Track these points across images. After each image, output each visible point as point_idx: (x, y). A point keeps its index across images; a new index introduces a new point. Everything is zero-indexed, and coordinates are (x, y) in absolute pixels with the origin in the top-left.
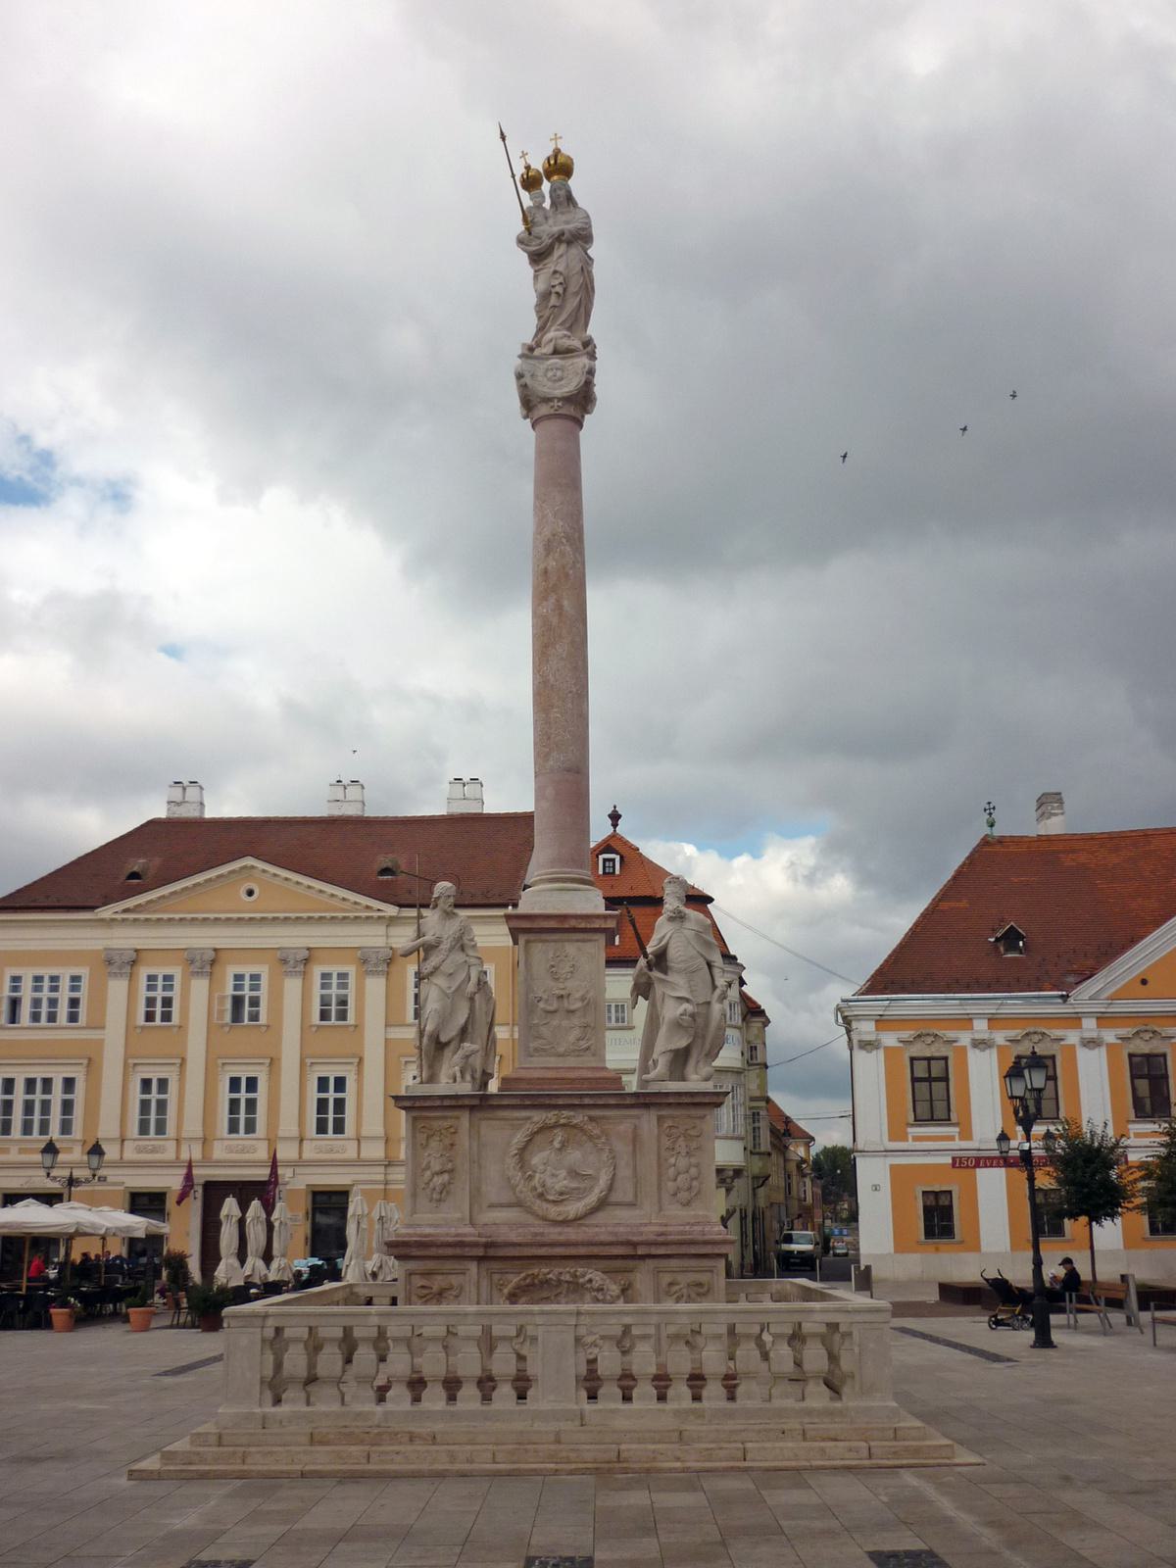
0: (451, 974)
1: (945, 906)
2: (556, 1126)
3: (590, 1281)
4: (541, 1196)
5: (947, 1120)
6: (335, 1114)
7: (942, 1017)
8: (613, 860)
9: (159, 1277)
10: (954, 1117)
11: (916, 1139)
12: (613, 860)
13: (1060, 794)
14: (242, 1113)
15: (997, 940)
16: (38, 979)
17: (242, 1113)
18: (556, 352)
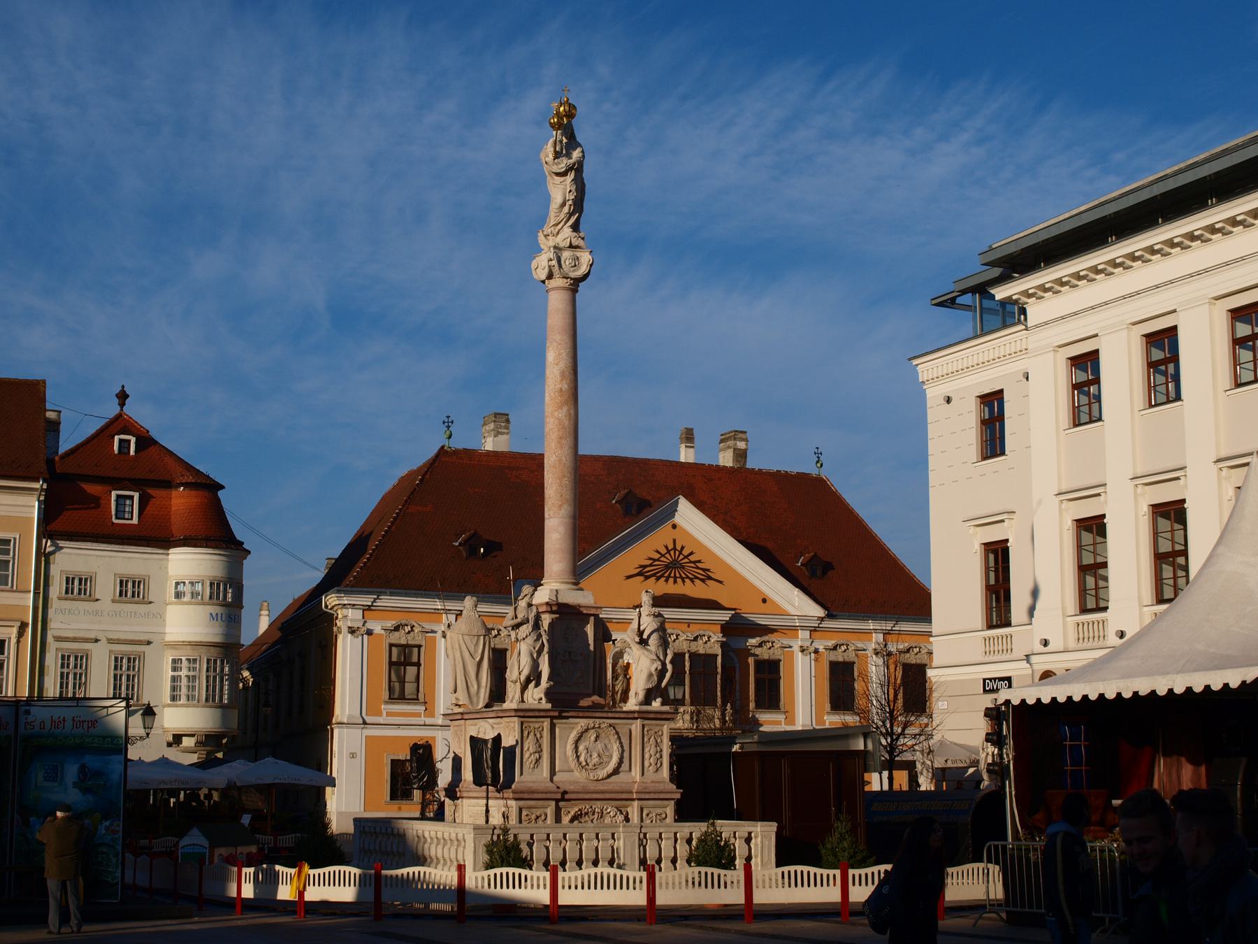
5: (415, 700)
7: (411, 610)
9: (512, 860)
10: (421, 696)
11: (389, 714)
13: (508, 415)
15: (460, 544)
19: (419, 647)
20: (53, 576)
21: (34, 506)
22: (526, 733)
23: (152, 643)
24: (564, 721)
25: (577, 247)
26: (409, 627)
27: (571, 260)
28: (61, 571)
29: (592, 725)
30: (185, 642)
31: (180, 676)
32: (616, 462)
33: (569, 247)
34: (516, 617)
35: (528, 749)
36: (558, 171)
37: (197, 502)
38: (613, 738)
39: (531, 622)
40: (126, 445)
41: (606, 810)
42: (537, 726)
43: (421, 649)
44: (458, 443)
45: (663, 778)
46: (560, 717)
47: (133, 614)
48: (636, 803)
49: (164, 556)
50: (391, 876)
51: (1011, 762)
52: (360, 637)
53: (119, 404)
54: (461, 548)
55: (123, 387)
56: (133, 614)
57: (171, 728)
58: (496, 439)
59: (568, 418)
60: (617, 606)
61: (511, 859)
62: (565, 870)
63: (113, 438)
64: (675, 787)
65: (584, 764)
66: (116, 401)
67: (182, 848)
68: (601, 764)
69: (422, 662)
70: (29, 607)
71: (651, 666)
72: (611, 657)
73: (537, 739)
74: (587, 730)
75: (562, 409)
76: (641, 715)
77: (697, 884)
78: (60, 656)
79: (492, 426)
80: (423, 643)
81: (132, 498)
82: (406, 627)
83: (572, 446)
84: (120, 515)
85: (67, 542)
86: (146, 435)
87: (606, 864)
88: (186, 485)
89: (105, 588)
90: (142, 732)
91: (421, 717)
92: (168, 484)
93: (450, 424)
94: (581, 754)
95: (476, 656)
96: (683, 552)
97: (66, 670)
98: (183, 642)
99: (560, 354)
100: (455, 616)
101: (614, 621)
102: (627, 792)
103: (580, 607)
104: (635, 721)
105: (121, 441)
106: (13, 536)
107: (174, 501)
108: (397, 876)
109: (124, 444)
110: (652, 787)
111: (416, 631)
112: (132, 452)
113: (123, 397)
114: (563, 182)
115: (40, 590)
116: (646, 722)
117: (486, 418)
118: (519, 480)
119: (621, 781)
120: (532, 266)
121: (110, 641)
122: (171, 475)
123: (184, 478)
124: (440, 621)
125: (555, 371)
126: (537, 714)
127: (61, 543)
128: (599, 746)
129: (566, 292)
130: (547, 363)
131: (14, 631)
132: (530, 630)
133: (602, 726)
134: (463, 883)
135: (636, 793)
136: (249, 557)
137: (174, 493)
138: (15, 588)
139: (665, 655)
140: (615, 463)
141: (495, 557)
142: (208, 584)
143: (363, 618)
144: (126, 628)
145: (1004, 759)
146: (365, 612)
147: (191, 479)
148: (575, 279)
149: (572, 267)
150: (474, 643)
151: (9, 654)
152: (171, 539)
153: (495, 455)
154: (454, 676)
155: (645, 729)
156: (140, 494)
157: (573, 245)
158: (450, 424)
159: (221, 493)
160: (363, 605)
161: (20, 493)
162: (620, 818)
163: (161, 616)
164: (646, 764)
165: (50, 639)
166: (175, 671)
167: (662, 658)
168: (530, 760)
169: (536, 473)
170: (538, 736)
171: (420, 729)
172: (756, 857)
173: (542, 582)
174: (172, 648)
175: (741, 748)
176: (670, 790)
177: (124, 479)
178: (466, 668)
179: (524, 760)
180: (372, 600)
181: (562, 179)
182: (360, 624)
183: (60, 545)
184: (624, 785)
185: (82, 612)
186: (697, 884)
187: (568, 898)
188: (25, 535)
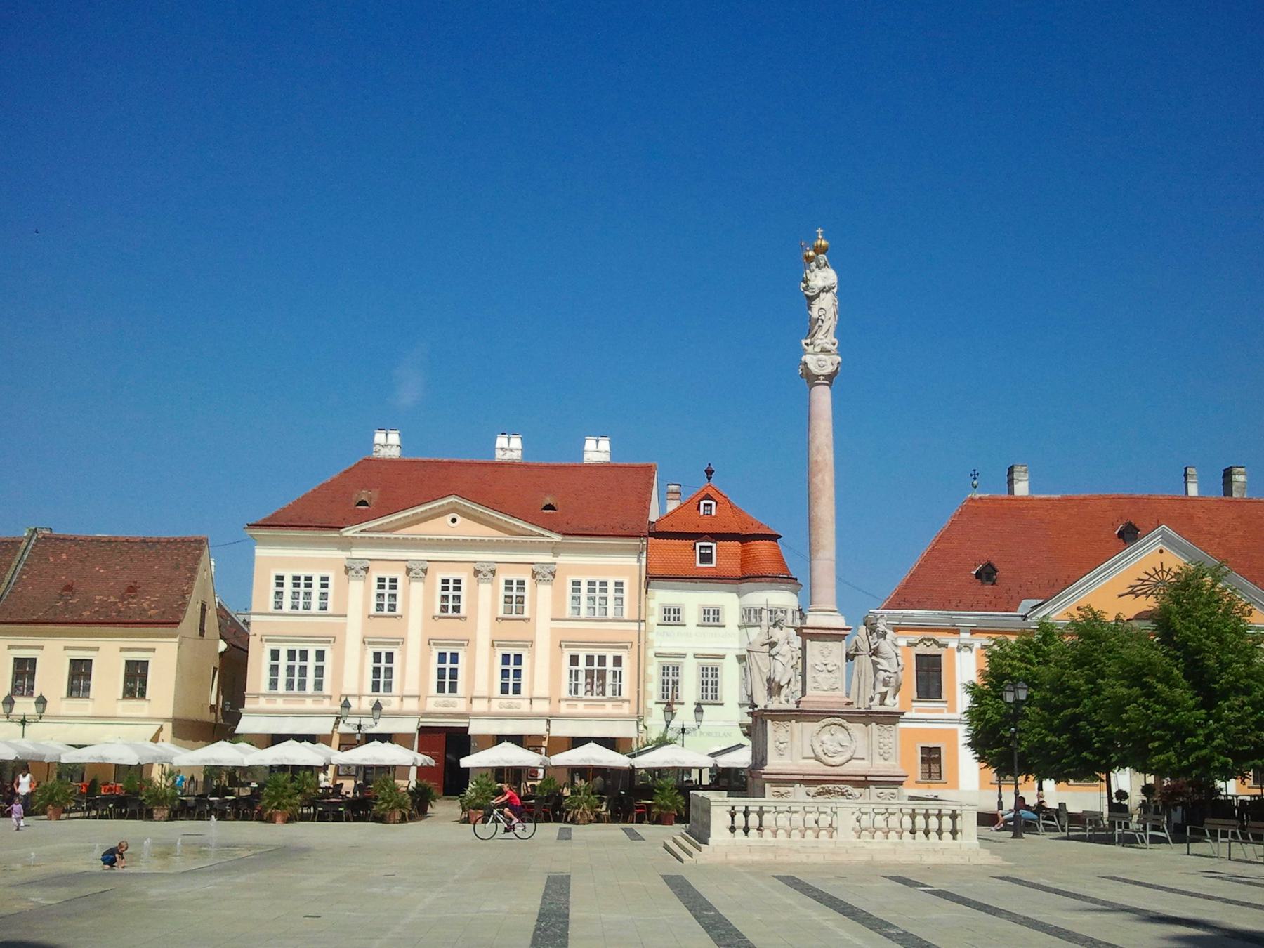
0: (784, 656)
1: (941, 545)
2: (831, 724)
3: (847, 791)
4: (825, 754)
8: (711, 505)
11: (918, 711)
12: (711, 505)
14: (447, 681)
16: (591, 583)
17: (447, 681)
18: (822, 351)
33: (821, 351)
89: (692, 615)
90: (695, 724)
96: (1152, 574)
121: (696, 656)
177: (705, 534)
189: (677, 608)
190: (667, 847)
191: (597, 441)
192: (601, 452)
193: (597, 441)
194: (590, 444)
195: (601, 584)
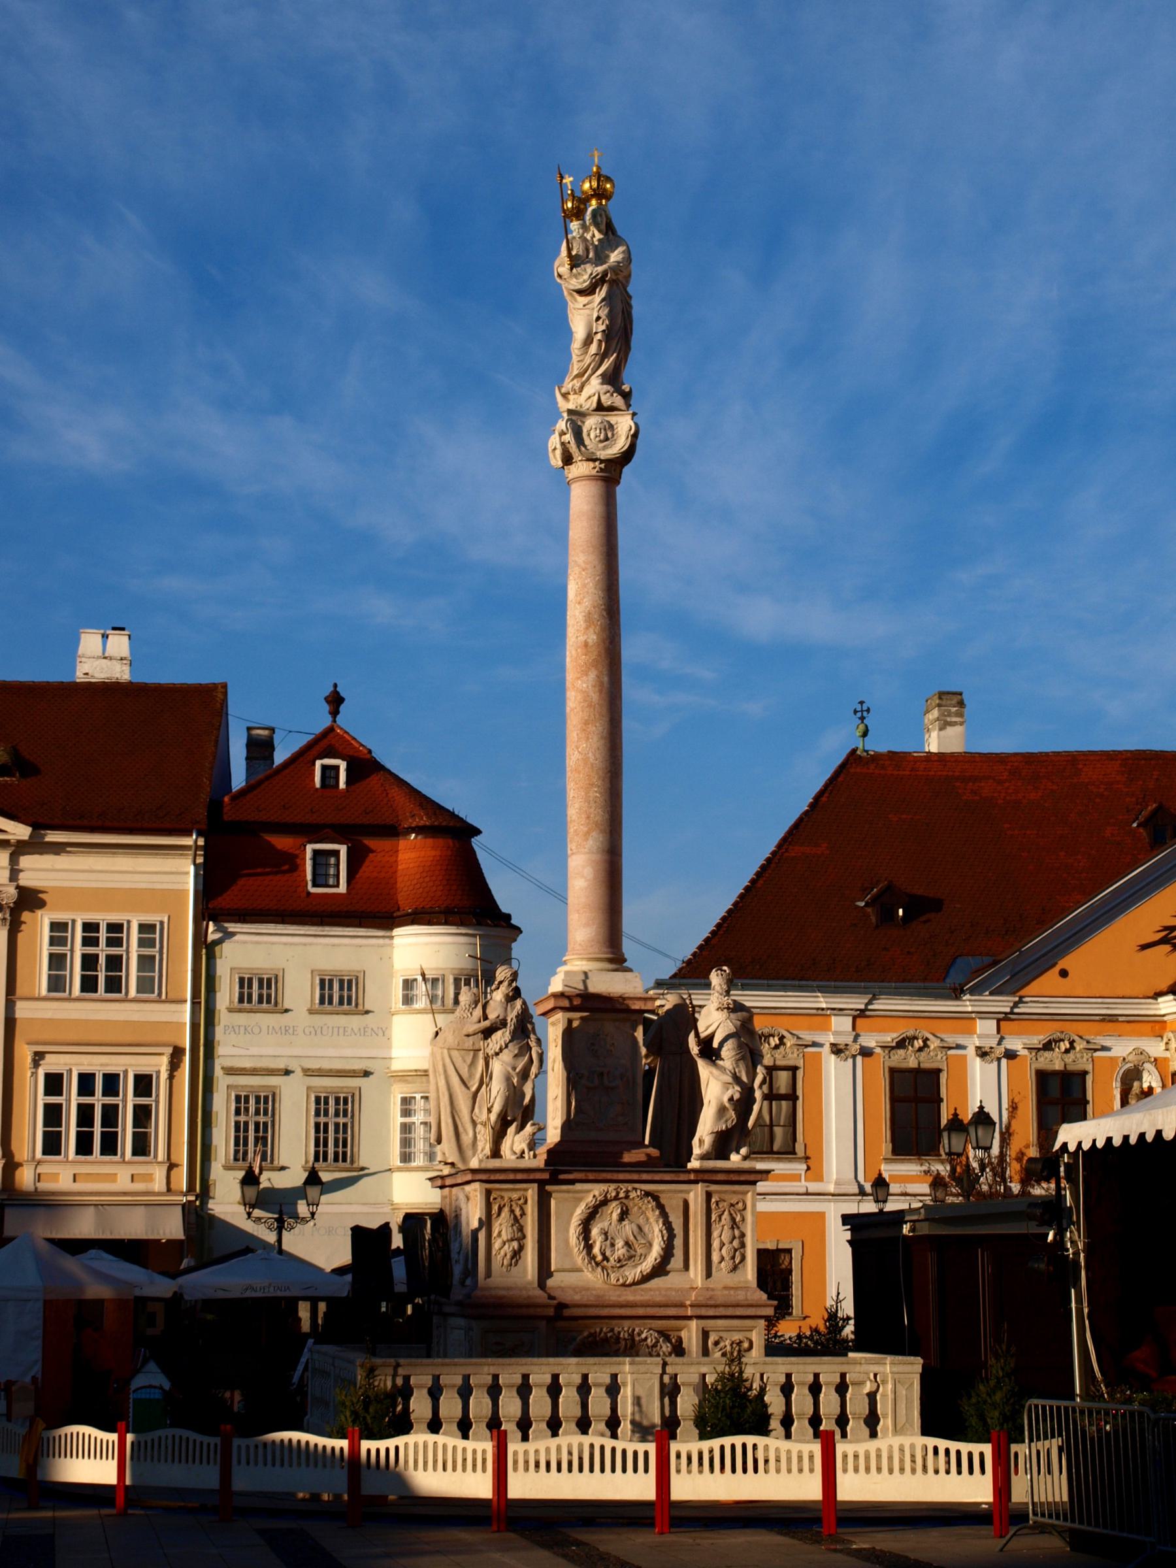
6: (102, 1126)
7: (778, 1011)
10: (799, 1148)
13: (961, 694)
15: (867, 904)
16: (90, 927)
19: (794, 1069)
20: (220, 977)
21: (188, 873)
22: (495, 1208)
23: (372, 1073)
24: (564, 1187)
25: (612, 409)
26: (776, 1039)
27: (598, 431)
28: (231, 969)
29: (614, 1194)
30: (420, 1071)
31: (414, 1123)
32: (1145, 759)
34: (486, 1018)
35: (499, 1234)
36: (579, 287)
37: (434, 856)
38: (653, 1215)
39: (511, 1026)
40: (333, 774)
41: (639, 1335)
42: (515, 1196)
43: (798, 1072)
44: (878, 744)
45: (747, 1281)
46: (555, 1181)
47: (341, 1030)
48: (694, 1324)
49: (387, 941)
50: (274, 1442)
51: (1082, 1255)
52: (996, 1063)
53: (330, 713)
54: (869, 910)
55: (335, 686)
56: (341, 1030)
57: (403, 1204)
58: (942, 733)
59: (597, 689)
60: (1128, 995)
61: (368, 1418)
62: (788, 1436)
63: (314, 764)
64: (765, 1296)
65: (599, 1258)
66: (326, 708)
67: (134, 1391)
68: (631, 1256)
69: (799, 1093)
70: (186, 1023)
71: (723, 1093)
72: (1119, 1080)
73: (515, 1217)
74: (605, 1202)
75: (587, 675)
76: (700, 1176)
77: (565, 1466)
78: (233, 1097)
79: (935, 713)
80: (800, 1063)
81: (336, 853)
82: (771, 1039)
83: (605, 734)
84: (320, 880)
85: (239, 925)
86: (368, 756)
87: (573, 1426)
88: (419, 830)
91: (800, 1181)
92: (393, 831)
93: (865, 714)
94: (594, 1242)
95: (472, 1083)
97: (242, 1118)
98: (416, 1071)
99: (584, 586)
100: (850, 1019)
101: (1121, 1019)
102: (675, 1306)
103: (624, 999)
104: (692, 1186)
105: (325, 768)
106: (159, 919)
107: (402, 856)
108: (282, 1441)
109: (330, 773)
110: (721, 1296)
111: (788, 1044)
112: (342, 785)
113: (335, 701)
114: (588, 304)
115: (200, 998)
116: (713, 1188)
117: (929, 701)
118: (977, 798)
119: (670, 1286)
120: (549, 446)
121: (308, 1073)
122: (397, 816)
123: (415, 820)
124: (826, 1028)
125: (577, 614)
126: (511, 1176)
127: (232, 927)
128: (628, 1228)
129: (593, 483)
130: (568, 603)
131: (163, 1063)
132: (508, 1037)
133: (633, 1195)
134: (356, 1450)
135: (691, 1306)
136: (521, 936)
137: (402, 843)
138: (164, 997)
139: (752, 1075)
140: (1143, 762)
141: (925, 922)
142: (451, 980)
143: (998, 1031)
144: (331, 1052)
145: (1067, 1250)
146: (1002, 1023)
147: (425, 821)
148: (608, 462)
149: (601, 441)
150: (469, 1060)
151: (158, 1096)
152: (395, 915)
153: (941, 758)
154: (437, 1115)
155: (713, 1200)
156: (348, 848)
157: (605, 405)
158: (865, 714)
159: (476, 842)
160: (852, 1009)
161: (168, 854)
162: (664, 1349)
163: (384, 1033)
164: (715, 1257)
165: (218, 1072)
166: (406, 1116)
167: (745, 1079)
168: (502, 1252)
169: (1007, 784)
170: (518, 1212)
171: (800, 1201)
172: (886, 1416)
173: (564, 959)
174: (400, 1081)
175: (912, 1230)
176: (754, 1303)
178: (455, 1103)
179: (494, 1253)
180: (1012, 1004)
181: (589, 298)
182: (993, 1042)
183: (230, 930)
184: (674, 1293)
185: (264, 1029)
186: (565, 1466)
187: (521, 1486)
188: (175, 918)
189: (246, 976)
190: (3, 1428)
191: (105, 637)
192: (111, 658)
193: (105, 637)
194: (90, 642)
195: (145, 928)
